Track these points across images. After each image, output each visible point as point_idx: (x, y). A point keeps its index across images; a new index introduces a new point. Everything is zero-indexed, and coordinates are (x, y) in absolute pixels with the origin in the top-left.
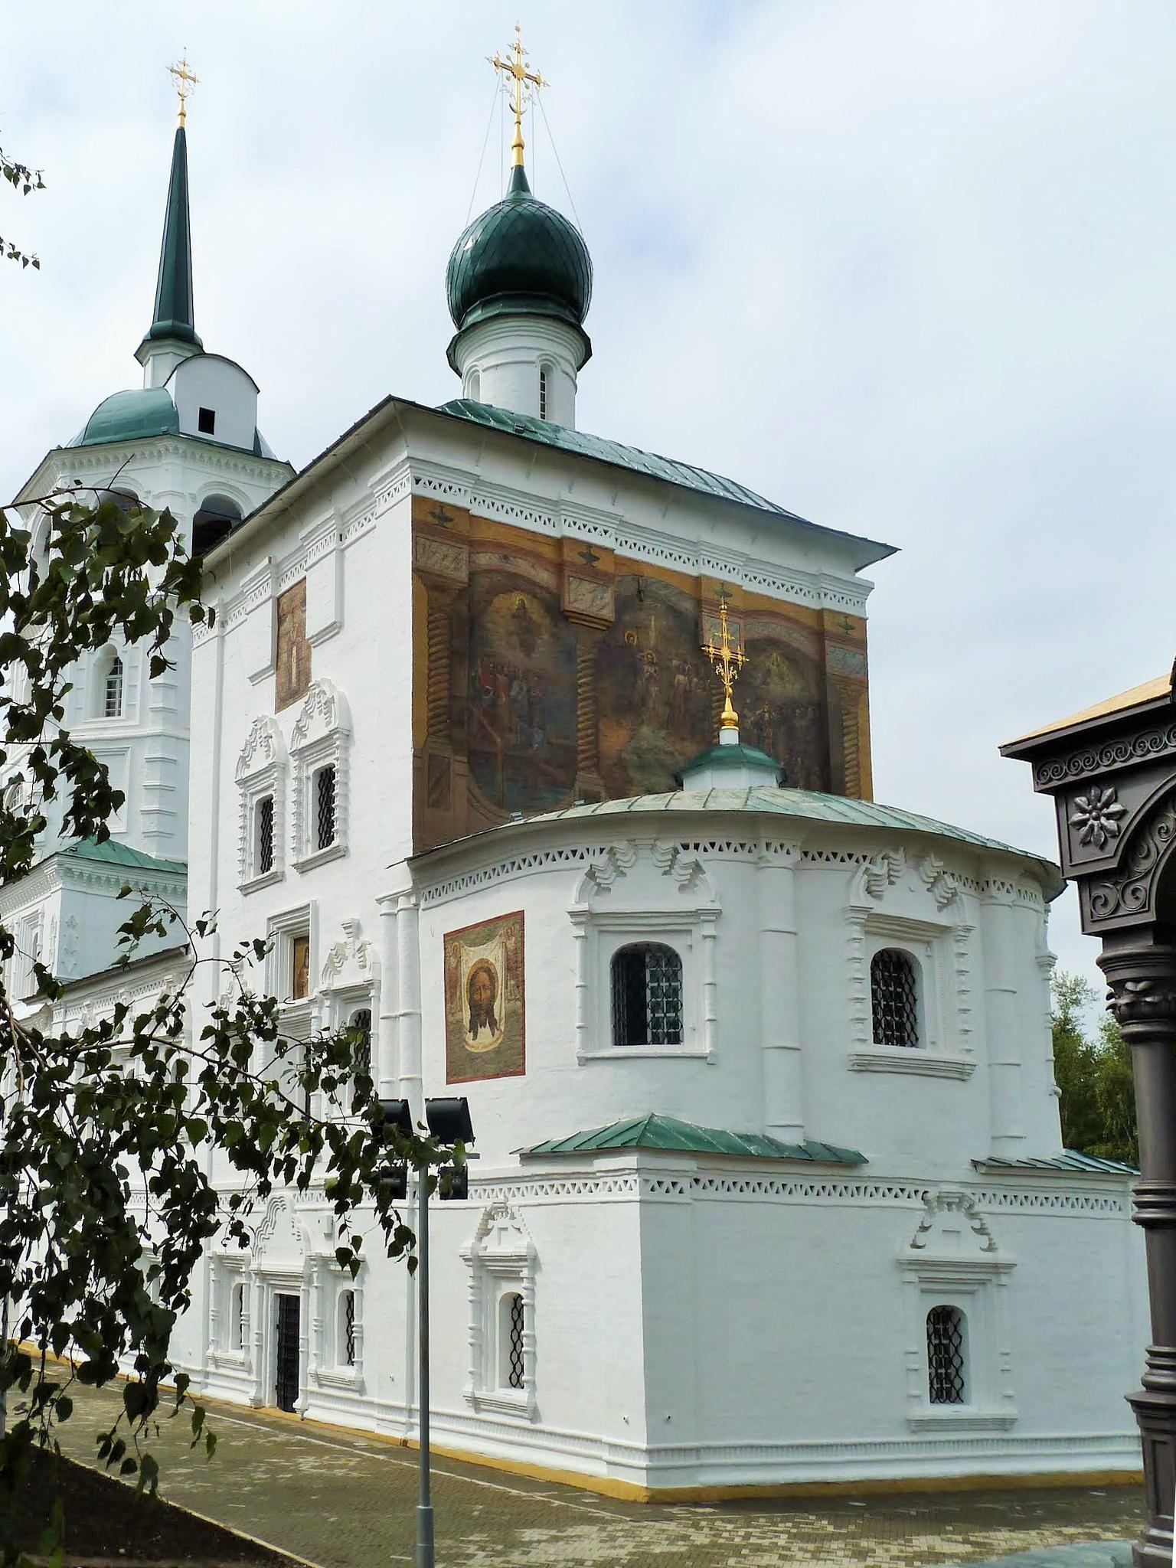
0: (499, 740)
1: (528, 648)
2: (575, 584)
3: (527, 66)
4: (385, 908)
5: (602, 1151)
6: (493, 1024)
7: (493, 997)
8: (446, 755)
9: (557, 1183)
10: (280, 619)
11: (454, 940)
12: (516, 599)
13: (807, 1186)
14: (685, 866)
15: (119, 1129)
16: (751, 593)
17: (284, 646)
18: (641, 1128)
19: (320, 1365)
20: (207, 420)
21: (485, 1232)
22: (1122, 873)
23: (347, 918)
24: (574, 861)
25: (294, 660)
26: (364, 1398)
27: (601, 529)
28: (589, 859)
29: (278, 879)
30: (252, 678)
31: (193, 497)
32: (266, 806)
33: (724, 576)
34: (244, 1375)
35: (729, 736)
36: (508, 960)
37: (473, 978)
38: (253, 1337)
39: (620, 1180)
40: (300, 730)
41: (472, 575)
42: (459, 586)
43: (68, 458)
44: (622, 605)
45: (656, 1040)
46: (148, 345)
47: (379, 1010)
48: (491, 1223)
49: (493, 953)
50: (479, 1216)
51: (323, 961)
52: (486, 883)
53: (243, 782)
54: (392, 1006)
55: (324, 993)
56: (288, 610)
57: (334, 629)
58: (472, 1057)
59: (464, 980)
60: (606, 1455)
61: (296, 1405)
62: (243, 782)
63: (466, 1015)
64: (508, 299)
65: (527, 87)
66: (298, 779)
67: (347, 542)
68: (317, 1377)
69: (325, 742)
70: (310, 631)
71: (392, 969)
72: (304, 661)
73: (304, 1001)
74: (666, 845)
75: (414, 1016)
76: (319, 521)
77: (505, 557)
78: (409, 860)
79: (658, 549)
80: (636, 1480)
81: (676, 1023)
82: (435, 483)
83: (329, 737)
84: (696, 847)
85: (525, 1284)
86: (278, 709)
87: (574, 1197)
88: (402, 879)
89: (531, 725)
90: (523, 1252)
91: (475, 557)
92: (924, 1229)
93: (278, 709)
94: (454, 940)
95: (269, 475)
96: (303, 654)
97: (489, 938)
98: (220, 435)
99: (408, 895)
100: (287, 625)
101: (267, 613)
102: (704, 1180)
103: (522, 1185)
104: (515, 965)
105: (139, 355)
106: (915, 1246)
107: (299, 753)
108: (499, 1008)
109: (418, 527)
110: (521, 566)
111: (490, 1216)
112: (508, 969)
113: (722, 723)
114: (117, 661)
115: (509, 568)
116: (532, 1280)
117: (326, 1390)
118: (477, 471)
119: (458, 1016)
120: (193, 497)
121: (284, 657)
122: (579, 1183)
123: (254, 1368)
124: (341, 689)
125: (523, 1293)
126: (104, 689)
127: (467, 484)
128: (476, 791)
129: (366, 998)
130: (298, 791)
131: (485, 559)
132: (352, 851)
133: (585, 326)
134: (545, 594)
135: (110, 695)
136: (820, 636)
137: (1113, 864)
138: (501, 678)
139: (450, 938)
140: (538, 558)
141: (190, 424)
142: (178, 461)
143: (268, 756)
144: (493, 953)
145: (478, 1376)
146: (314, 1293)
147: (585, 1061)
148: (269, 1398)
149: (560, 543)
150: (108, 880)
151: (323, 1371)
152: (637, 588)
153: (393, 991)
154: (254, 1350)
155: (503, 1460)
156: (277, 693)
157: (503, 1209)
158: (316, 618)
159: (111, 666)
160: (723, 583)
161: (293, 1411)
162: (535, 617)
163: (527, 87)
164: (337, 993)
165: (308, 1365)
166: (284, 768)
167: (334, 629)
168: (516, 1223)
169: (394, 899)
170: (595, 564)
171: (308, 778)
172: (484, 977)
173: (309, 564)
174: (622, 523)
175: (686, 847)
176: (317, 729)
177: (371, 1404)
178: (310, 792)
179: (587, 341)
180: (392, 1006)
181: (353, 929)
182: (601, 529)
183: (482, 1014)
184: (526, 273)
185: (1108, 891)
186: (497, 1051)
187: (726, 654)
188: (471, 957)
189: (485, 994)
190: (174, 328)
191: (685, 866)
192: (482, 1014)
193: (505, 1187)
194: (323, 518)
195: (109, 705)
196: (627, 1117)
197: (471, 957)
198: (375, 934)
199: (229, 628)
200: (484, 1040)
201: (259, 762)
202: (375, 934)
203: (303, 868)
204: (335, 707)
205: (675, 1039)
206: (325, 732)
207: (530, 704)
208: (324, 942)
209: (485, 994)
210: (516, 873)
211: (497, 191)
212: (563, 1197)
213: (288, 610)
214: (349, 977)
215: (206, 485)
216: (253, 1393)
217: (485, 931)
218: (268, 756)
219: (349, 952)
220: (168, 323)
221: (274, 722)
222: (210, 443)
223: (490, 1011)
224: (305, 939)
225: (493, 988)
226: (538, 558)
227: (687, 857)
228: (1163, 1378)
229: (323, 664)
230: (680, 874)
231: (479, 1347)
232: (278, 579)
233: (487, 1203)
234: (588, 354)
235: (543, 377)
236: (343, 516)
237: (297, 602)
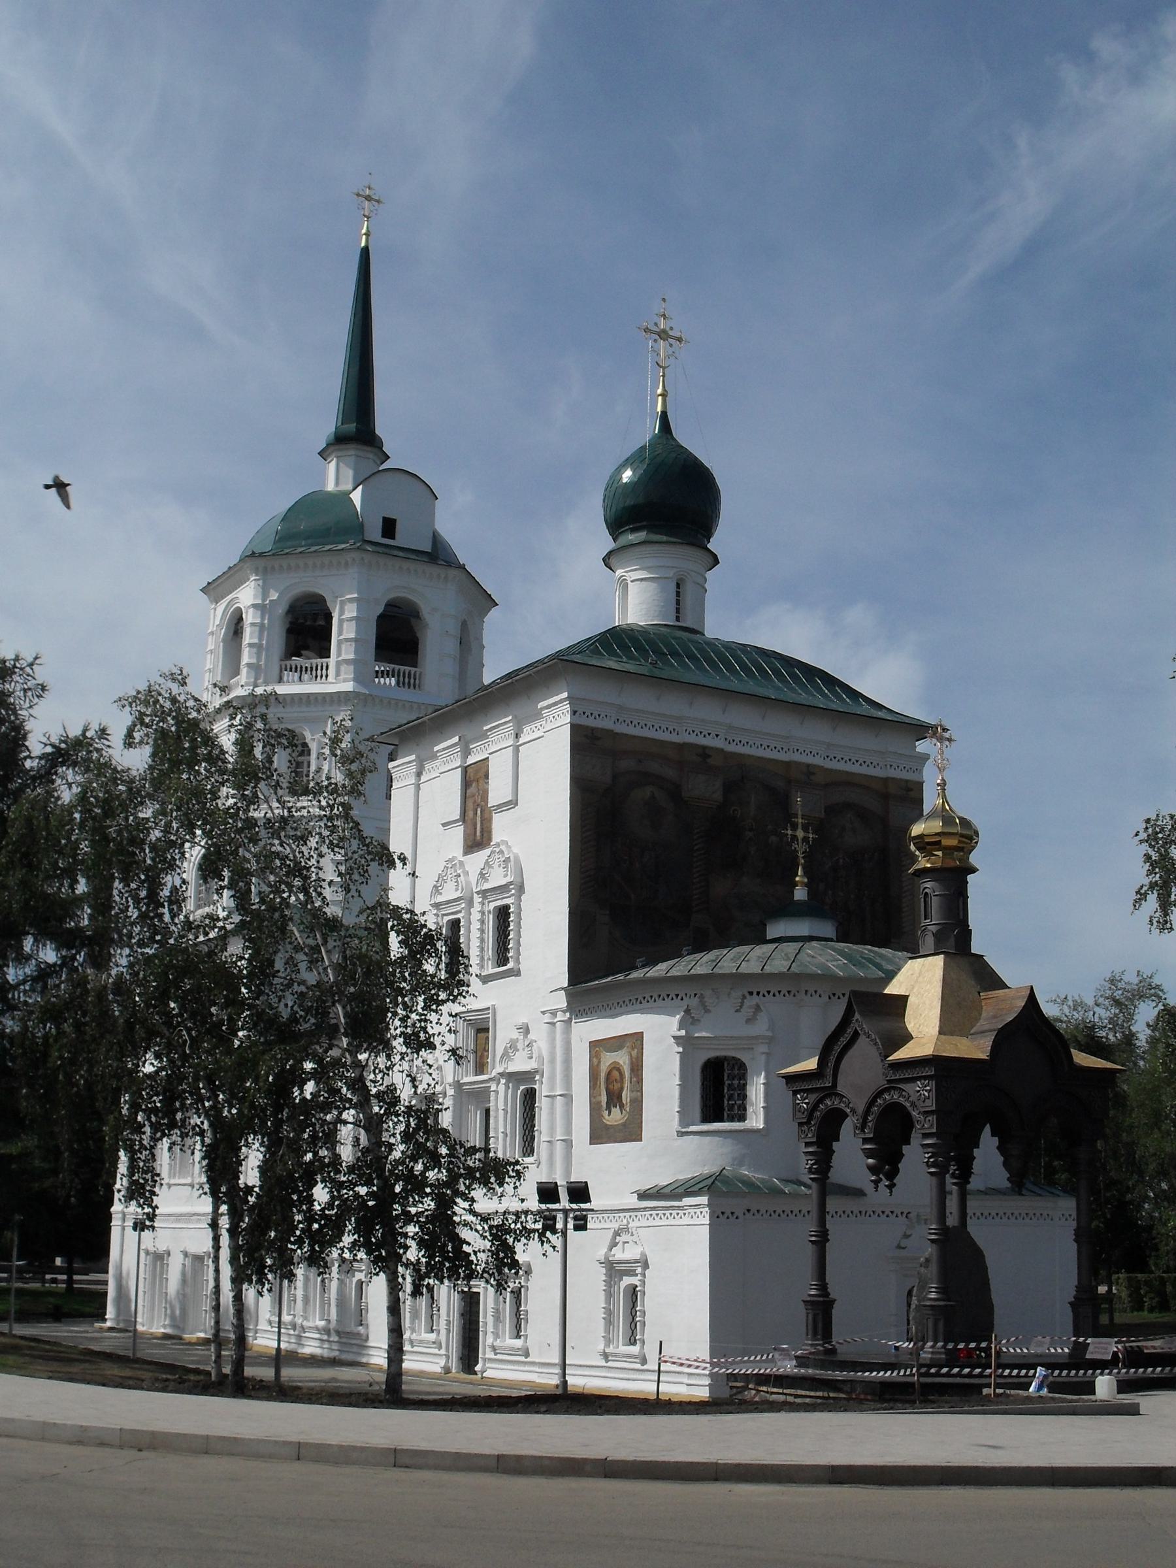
3: (671, 328)
5: (689, 1193)
6: (622, 1106)
7: (622, 1089)
10: (466, 784)
11: (597, 1047)
12: (648, 791)
14: (750, 1007)
16: (831, 770)
17: (470, 804)
18: (711, 1180)
19: (495, 1339)
20: (389, 527)
21: (614, 1244)
22: (808, 1123)
23: (523, 1020)
24: (677, 1001)
25: (479, 819)
26: (528, 1359)
28: (686, 1001)
30: (444, 825)
33: (809, 760)
34: (436, 1351)
35: (800, 894)
36: (632, 1063)
37: (609, 1074)
38: (443, 1323)
39: (698, 1211)
40: (483, 876)
44: (730, 788)
45: (731, 1120)
46: (332, 448)
47: (542, 1090)
49: (622, 1058)
51: (499, 1051)
54: (552, 1088)
55: (501, 1075)
56: (474, 780)
59: (603, 1075)
60: (686, 1381)
61: (478, 1368)
63: (604, 1099)
64: (651, 529)
65: (671, 345)
66: (483, 913)
68: (494, 1349)
69: (503, 889)
70: (493, 800)
71: (553, 1061)
73: (484, 1077)
74: (737, 994)
75: (568, 1097)
80: (703, 1393)
84: (758, 993)
85: (639, 1277)
87: (671, 1221)
88: (561, 1001)
90: (638, 1257)
92: (906, 1236)
95: (446, 577)
96: (486, 816)
97: (620, 1048)
98: (401, 539)
99: (564, 1012)
100: (472, 790)
101: (455, 780)
103: (639, 1214)
104: (637, 1067)
106: (899, 1247)
107: (484, 893)
108: (626, 1096)
111: (617, 1234)
112: (632, 1070)
113: (795, 884)
116: (644, 1276)
117: (499, 1357)
119: (598, 1099)
121: (470, 814)
122: (674, 1212)
123: (444, 1345)
124: (515, 850)
125: (638, 1283)
136: (885, 797)
139: (594, 1045)
141: (374, 533)
143: (457, 890)
144: (622, 1058)
145: (608, 1341)
146: (491, 1290)
147: (681, 1134)
148: (454, 1365)
151: (498, 1343)
152: (739, 775)
153: (552, 1078)
154: (443, 1332)
155: (623, 1391)
156: (465, 840)
157: (626, 1229)
158: (498, 790)
160: (808, 766)
161: (475, 1373)
163: (671, 345)
165: (487, 1339)
166: (470, 903)
167: (513, 803)
168: (635, 1238)
169: (554, 1013)
170: (709, 760)
171: (489, 912)
172: (616, 1074)
175: (751, 993)
176: (497, 878)
177: (533, 1363)
178: (490, 920)
180: (552, 1088)
181: (525, 1030)
183: (614, 1099)
184: (670, 504)
185: (805, 1128)
186: (624, 1125)
187: (800, 834)
188: (608, 1059)
189: (617, 1086)
190: (357, 430)
191: (750, 1007)
192: (614, 1099)
193: (628, 1215)
196: (707, 1170)
198: (539, 1034)
199: (423, 779)
200: (615, 1117)
201: (450, 892)
202: (539, 1034)
204: (511, 865)
205: (742, 1118)
206: (503, 882)
208: (503, 1034)
212: (664, 1222)
213: (474, 780)
214: (520, 1064)
216: (442, 1362)
217: (616, 1043)
218: (457, 890)
219: (520, 1046)
221: (461, 863)
223: (620, 1097)
224: (487, 1030)
227: (755, 1000)
229: (501, 827)
230: (747, 1011)
231: (609, 1321)
233: (616, 1226)
235: (678, 586)
237: (481, 774)
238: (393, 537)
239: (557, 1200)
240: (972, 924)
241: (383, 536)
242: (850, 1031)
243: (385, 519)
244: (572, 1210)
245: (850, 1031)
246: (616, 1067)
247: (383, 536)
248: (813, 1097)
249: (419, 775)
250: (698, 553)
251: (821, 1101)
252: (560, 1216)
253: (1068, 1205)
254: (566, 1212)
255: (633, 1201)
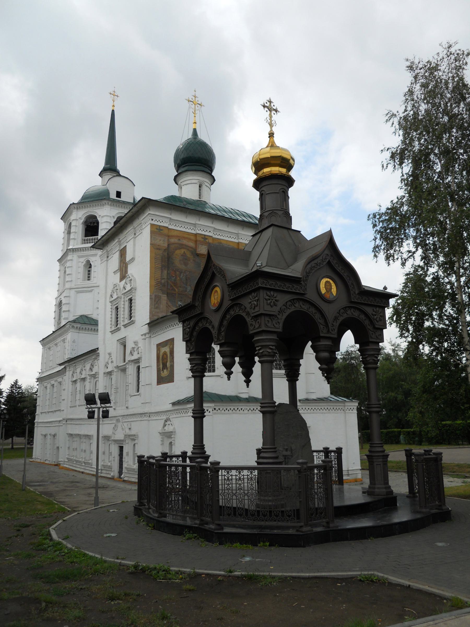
0: (177, 290)
1: (186, 264)
2: (200, 246)
4: (144, 337)
6: (167, 369)
7: (167, 362)
8: (160, 294)
9: (180, 411)
12: (182, 251)
13: (248, 409)
15: (438, 382)
20: (119, 194)
21: (165, 425)
27: (208, 231)
29: (119, 329)
31: (114, 217)
32: (117, 308)
37: (163, 356)
40: (124, 288)
41: (168, 245)
42: (165, 248)
43: (76, 206)
48: (166, 423)
49: (166, 349)
50: (163, 421)
52: (166, 330)
53: (111, 302)
55: (129, 361)
57: (133, 260)
58: (162, 378)
59: (161, 357)
62: (111, 302)
66: (124, 301)
67: (136, 235)
72: (126, 268)
76: (129, 229)
77: (179, 239)
78: (148, 324)
79: (226, 235)
81: (214, 366)
82: (158, 220)
83: (131, 290)
86: (120, 281)
88: (146, 329)
89: (186, 285)
91: (170, 240)
93: (120, 281)
94: (159, 346)
97: (166, 345)
98: (123, 198)
99: (148, 333)
100: (122, 258)
102: (217, 408)
105: (100, 175)
108: (168, 364)
109: (152, 232)
110: (185, 242)
111: (166, 421)
114: (91, 264)
115: (180, 242)
118: (170, 216)
120: (114, 217)
126: (87, 273)
127: (167, 220)
128: (170, 304)
129: (139, 362)
130: (124, 305)
131: (172, 240)
132: (136, 323)
133: (213, 174)
134: (191, 249)
135: (89, 274)
137: (188, 339)
138: (178, 273)
140: (190, 240)
141: (113, 195)
142: (109, 207)
149: (196, 235)
150: (86, 329)
159: (89, 266)
162: (188, 256)
164: (132, 361)
167: (133, 260)
169: (145, 335)
172: (165, 356)
173: (128, 240)
174: (215, 229)
178: (127, 304)
179: (213, 177)
181: (136, 343)
182: (208, 231)
183: (165, 366)
189: (165, 361)
192: (165, 366)
194: (130, 230)
195: (89, 277)
197: (163, 350)
199: (109, 258)
200: (165, 373)
201: (115, 296)
203: (125, 326)
204: (132, 281)
205: (214, 371)
207: (186, 279)
208: (130, 345)
209: (165, 361)
210: (172, 328)
211: (189, 135)
213: (123, 253)
215: (117, 213)
220: (109, 166)
222: (119, 201)
223: (166, 366)
225: (167, 359)
226: (190, 240)
228: (196, 451)
232: (120, 245)
234: (214, 180)
235: (200, 187)
236: (135, 228)
238: (120, 198)
239: (95, 403)
240: (292, 213)
241: (117, 197)
242: (210, 274)
243: (117, 192)
244: (102, 407)
245: (210, 274)
246: (165, 353)
247: (117, 197)
248: (192, 323)
249: (108, 257)
250: (208, 176)
251: (196, 324)
252: (96, 410)
253: (355, 404)
254: (99, 408)
255: (170, 407)
